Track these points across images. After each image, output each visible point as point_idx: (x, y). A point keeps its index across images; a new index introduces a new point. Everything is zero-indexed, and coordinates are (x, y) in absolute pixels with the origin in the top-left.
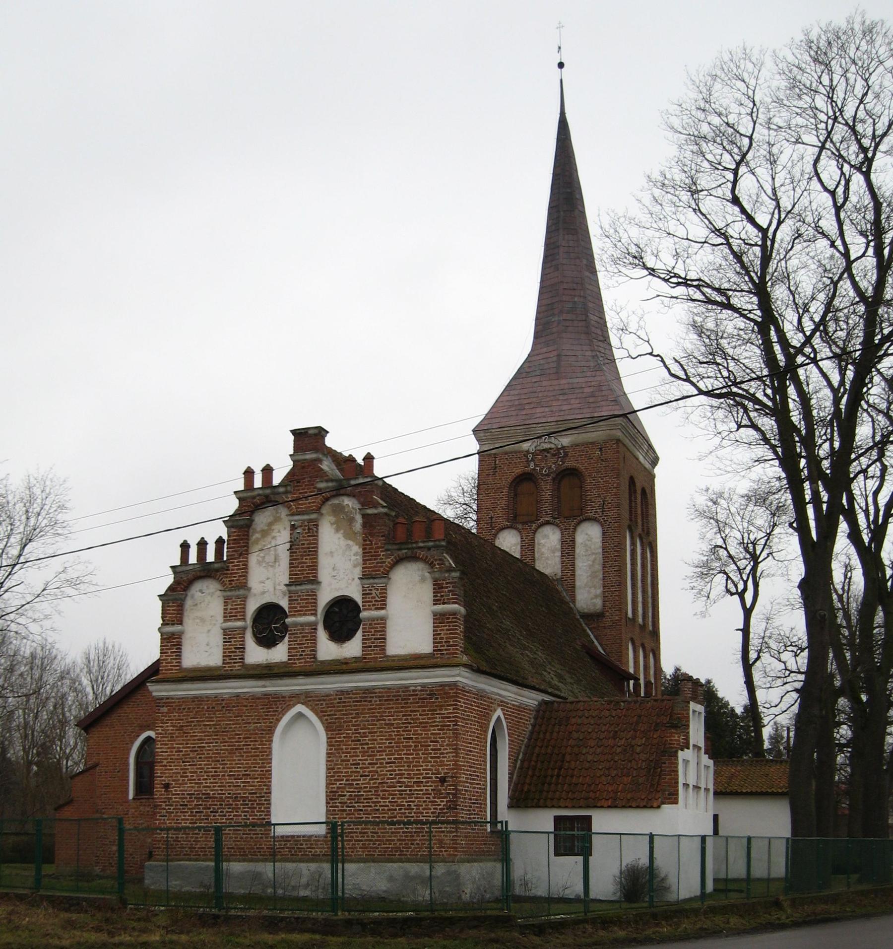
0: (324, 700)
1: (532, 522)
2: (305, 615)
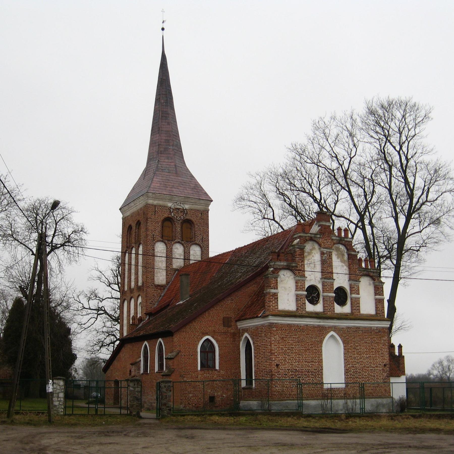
1: (172, 240)
2: (330, 292)
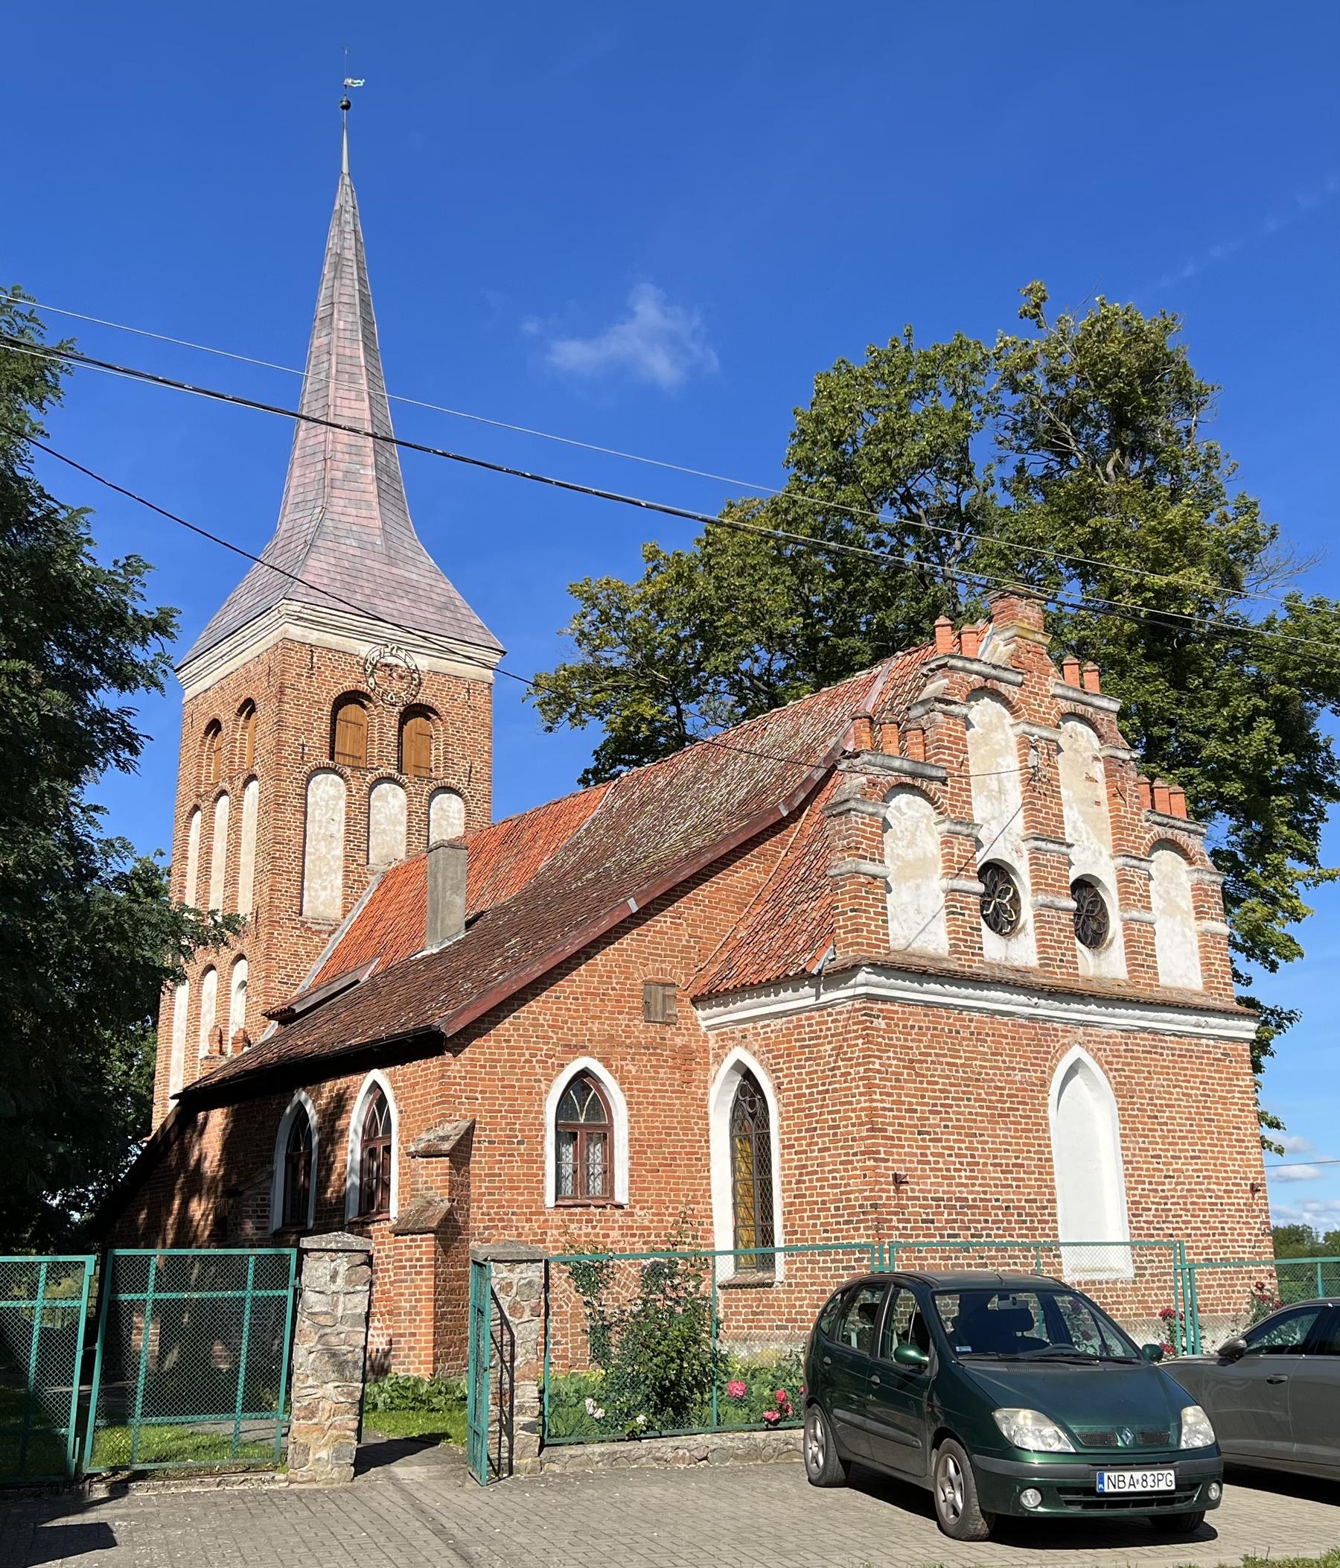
0: (1108, 1043)
